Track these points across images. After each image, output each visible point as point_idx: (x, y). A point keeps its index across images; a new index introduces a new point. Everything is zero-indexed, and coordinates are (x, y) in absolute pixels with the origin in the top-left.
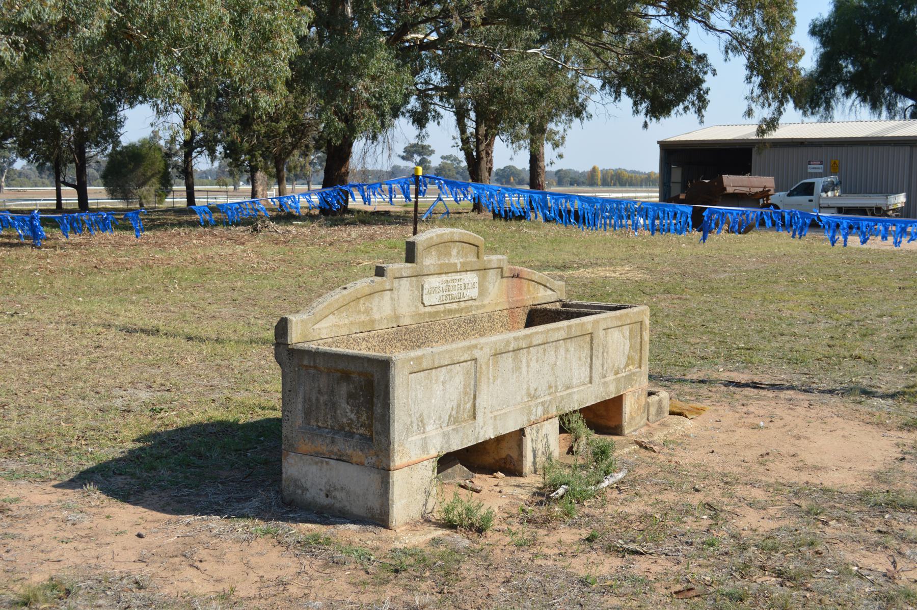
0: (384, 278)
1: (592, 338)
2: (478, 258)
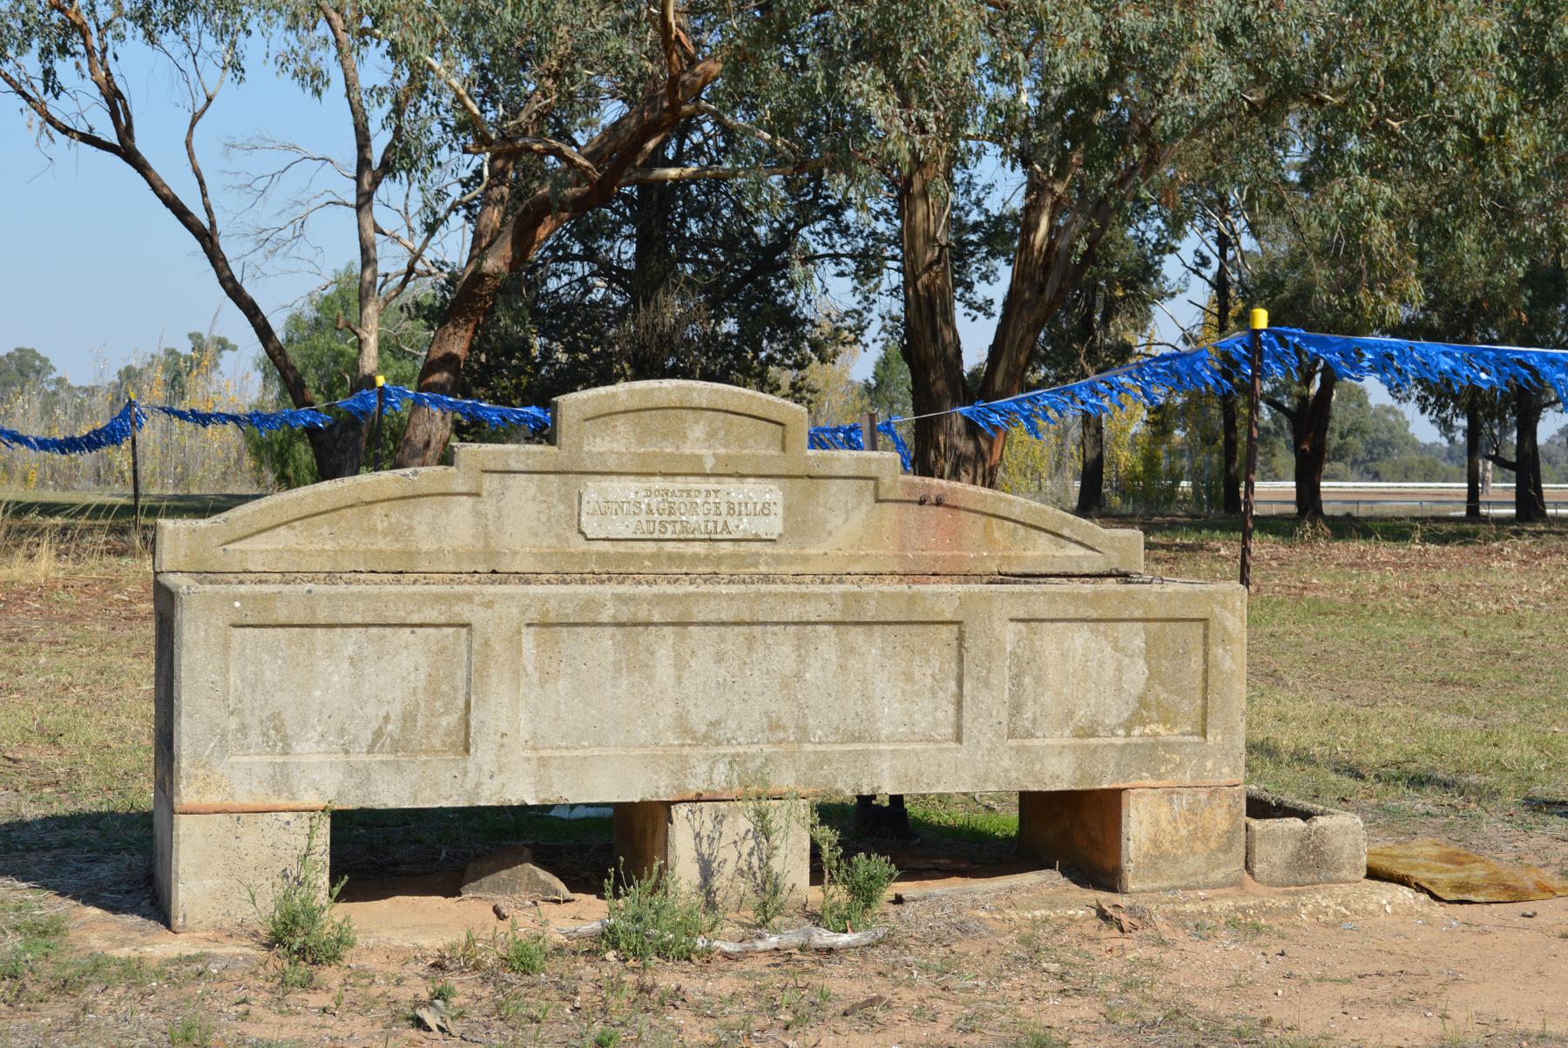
0: (452, 470)
1: (961, 638)
2: (784, 449)
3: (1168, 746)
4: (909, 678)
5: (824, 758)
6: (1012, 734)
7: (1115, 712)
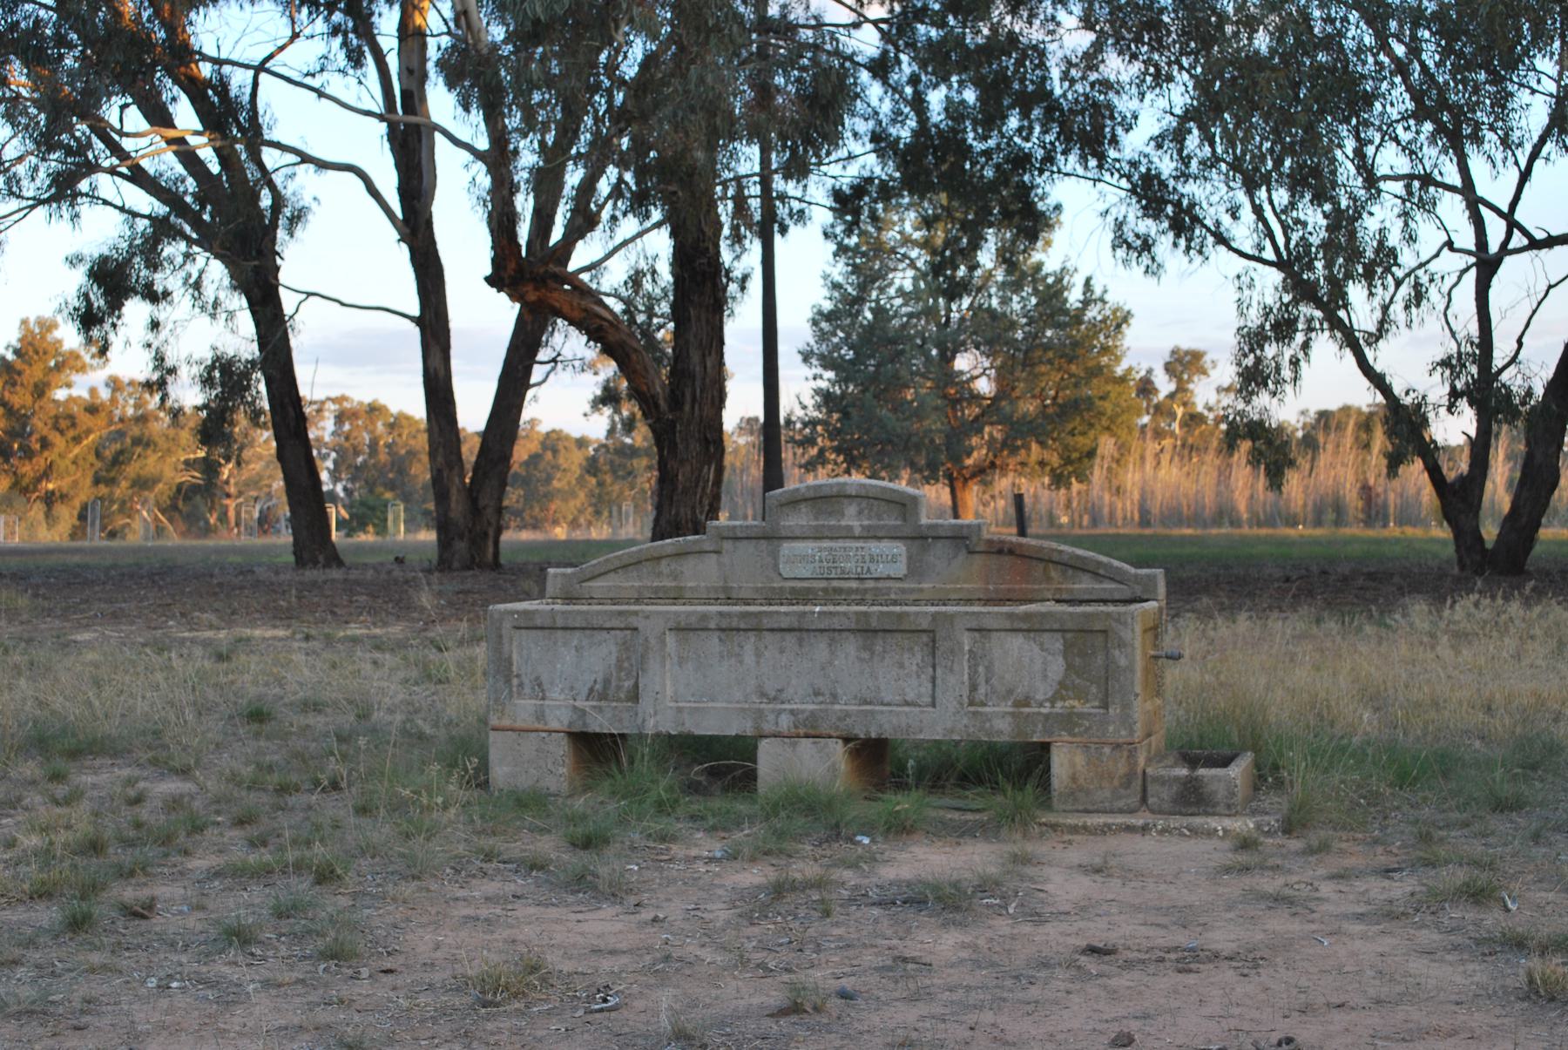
3: (1081, 716)
4: (901, 666)
5: (847, 714)
6: (971, 704)
7: (1043, 691)
